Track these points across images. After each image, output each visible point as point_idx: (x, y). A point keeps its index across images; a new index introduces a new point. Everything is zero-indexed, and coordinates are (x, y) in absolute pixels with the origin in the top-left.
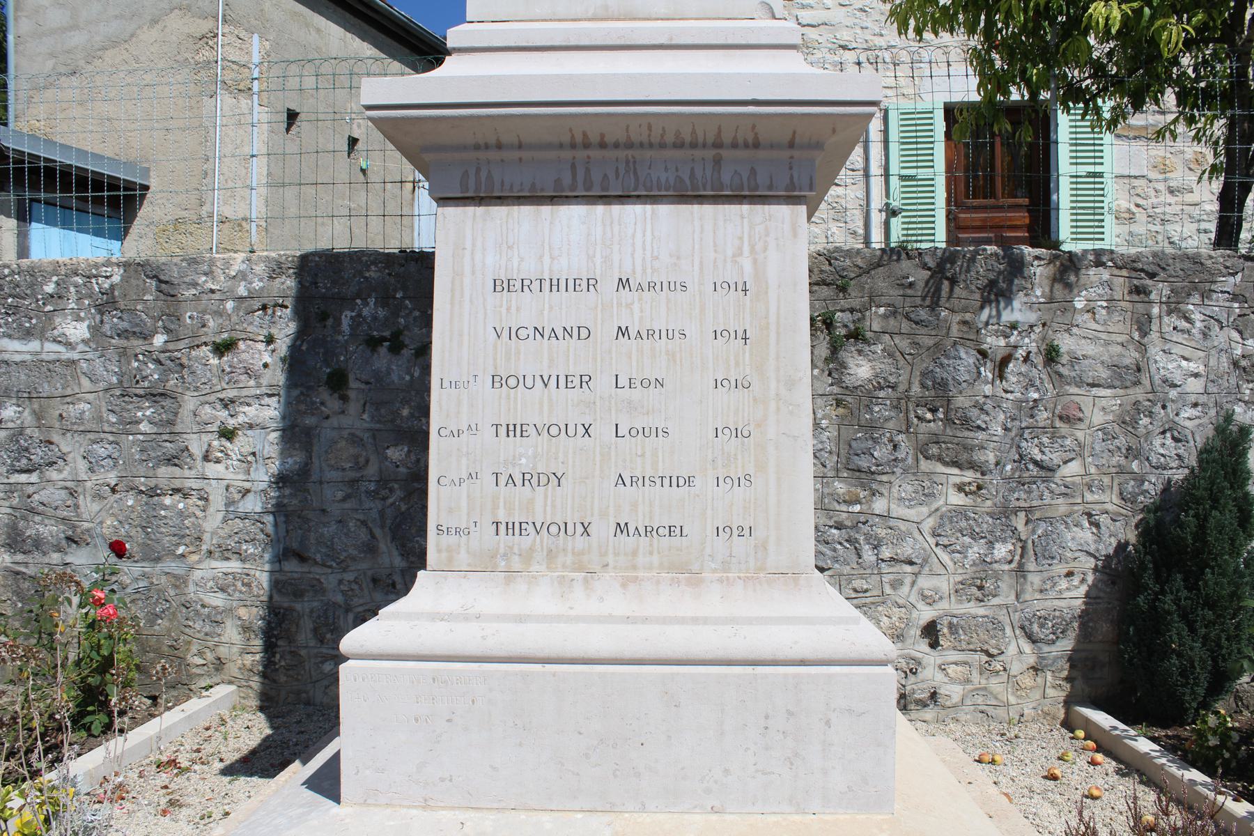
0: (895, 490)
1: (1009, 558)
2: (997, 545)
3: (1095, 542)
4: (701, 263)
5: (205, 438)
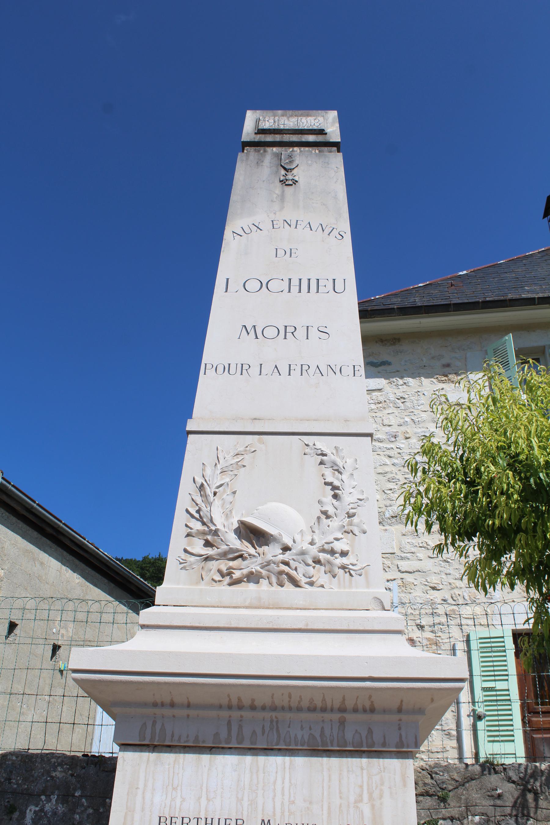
4: (329, 808)
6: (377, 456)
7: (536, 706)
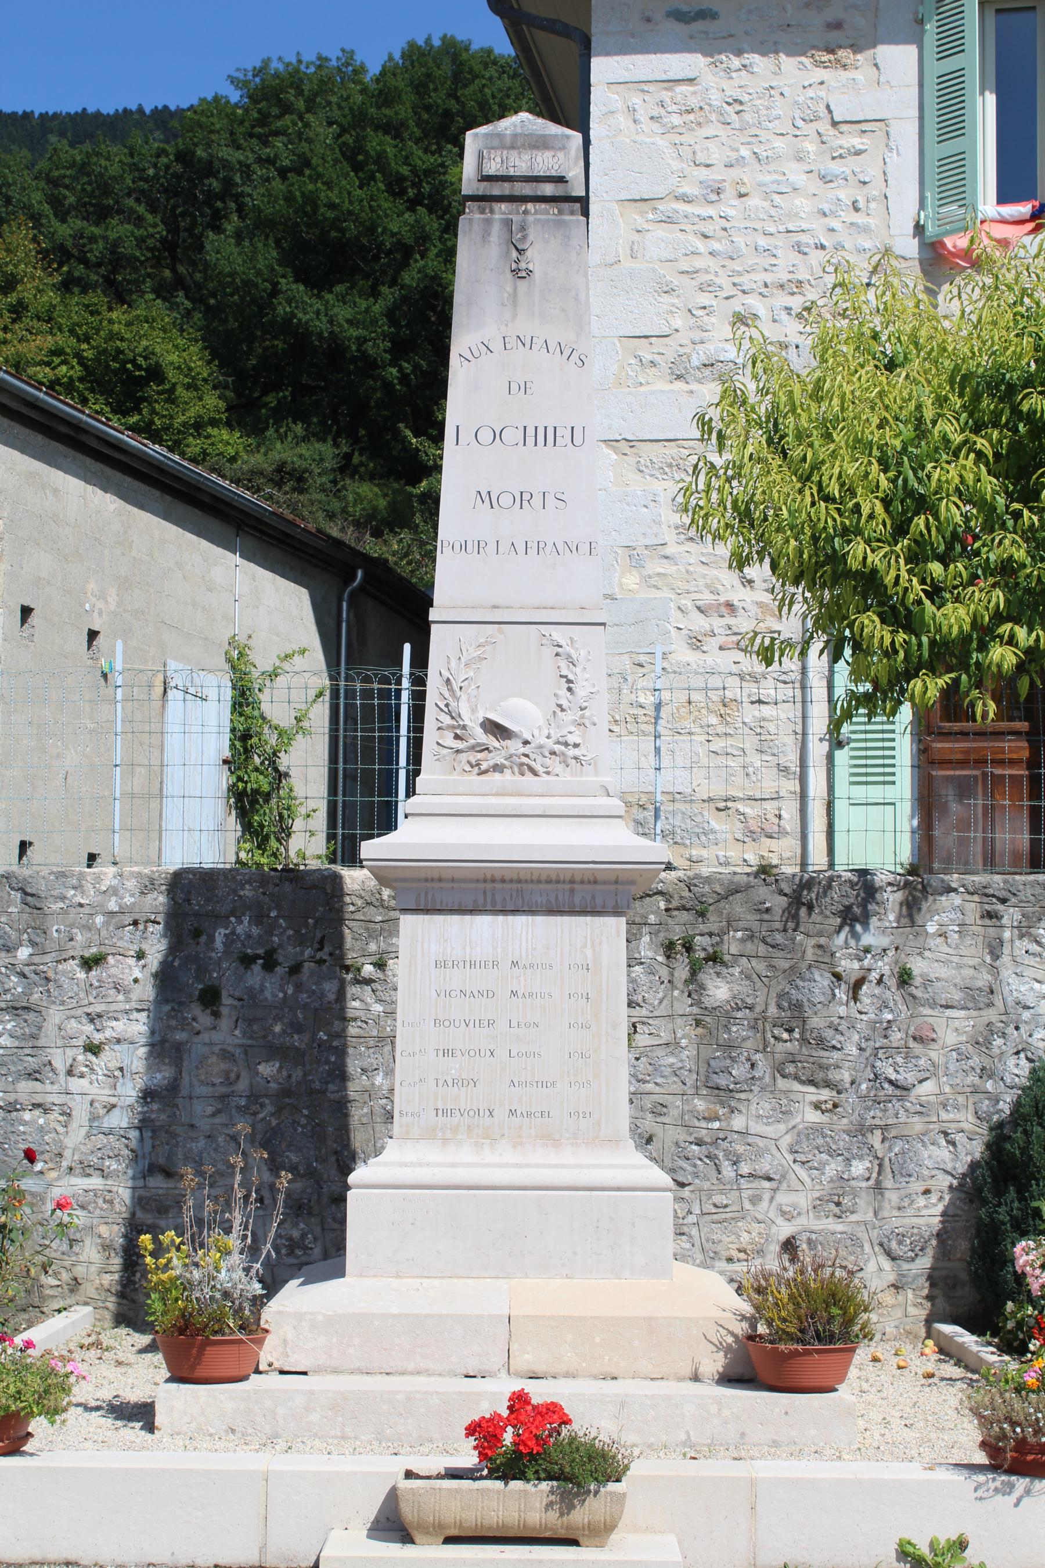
1: (867, 1175)
2: (854, 1163)
3: (953, 1160)
5: (70, 1053)
6: (679, 235)
7: (942, 720)
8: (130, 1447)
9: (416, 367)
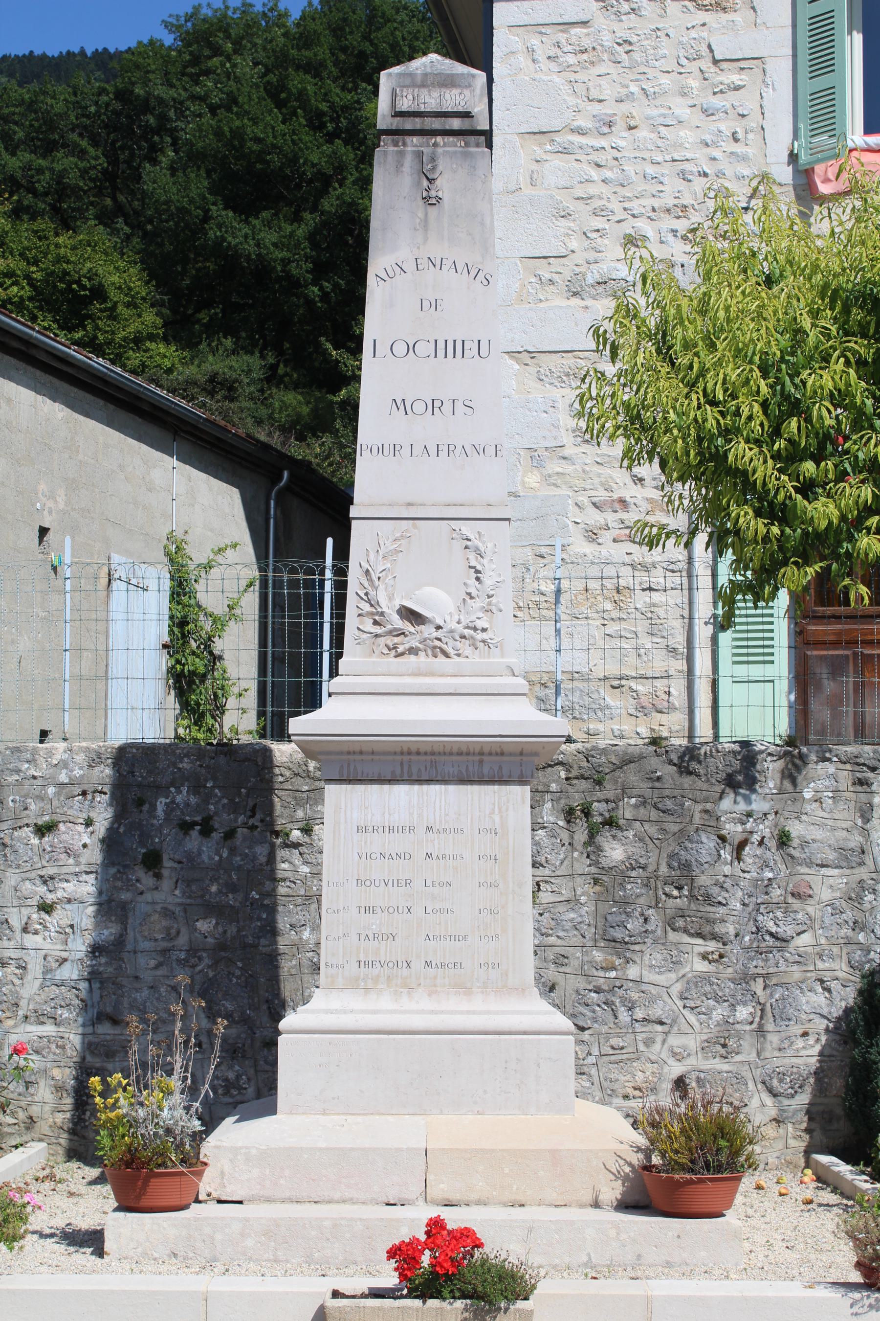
0: (647, 957)
1: (750, 1020)
2: (739, 1008)
5: (25, 911)
6: (575, 164)
7: (816, 605)
8: (81, 1270)
9: (336, 286)
